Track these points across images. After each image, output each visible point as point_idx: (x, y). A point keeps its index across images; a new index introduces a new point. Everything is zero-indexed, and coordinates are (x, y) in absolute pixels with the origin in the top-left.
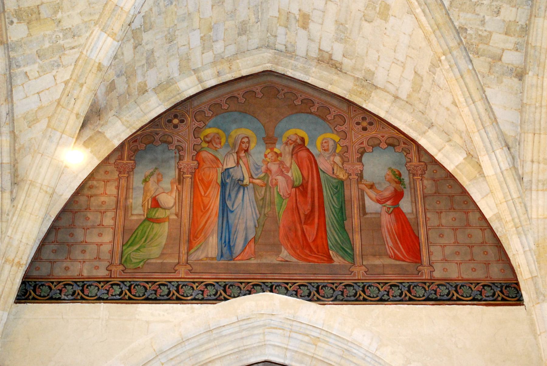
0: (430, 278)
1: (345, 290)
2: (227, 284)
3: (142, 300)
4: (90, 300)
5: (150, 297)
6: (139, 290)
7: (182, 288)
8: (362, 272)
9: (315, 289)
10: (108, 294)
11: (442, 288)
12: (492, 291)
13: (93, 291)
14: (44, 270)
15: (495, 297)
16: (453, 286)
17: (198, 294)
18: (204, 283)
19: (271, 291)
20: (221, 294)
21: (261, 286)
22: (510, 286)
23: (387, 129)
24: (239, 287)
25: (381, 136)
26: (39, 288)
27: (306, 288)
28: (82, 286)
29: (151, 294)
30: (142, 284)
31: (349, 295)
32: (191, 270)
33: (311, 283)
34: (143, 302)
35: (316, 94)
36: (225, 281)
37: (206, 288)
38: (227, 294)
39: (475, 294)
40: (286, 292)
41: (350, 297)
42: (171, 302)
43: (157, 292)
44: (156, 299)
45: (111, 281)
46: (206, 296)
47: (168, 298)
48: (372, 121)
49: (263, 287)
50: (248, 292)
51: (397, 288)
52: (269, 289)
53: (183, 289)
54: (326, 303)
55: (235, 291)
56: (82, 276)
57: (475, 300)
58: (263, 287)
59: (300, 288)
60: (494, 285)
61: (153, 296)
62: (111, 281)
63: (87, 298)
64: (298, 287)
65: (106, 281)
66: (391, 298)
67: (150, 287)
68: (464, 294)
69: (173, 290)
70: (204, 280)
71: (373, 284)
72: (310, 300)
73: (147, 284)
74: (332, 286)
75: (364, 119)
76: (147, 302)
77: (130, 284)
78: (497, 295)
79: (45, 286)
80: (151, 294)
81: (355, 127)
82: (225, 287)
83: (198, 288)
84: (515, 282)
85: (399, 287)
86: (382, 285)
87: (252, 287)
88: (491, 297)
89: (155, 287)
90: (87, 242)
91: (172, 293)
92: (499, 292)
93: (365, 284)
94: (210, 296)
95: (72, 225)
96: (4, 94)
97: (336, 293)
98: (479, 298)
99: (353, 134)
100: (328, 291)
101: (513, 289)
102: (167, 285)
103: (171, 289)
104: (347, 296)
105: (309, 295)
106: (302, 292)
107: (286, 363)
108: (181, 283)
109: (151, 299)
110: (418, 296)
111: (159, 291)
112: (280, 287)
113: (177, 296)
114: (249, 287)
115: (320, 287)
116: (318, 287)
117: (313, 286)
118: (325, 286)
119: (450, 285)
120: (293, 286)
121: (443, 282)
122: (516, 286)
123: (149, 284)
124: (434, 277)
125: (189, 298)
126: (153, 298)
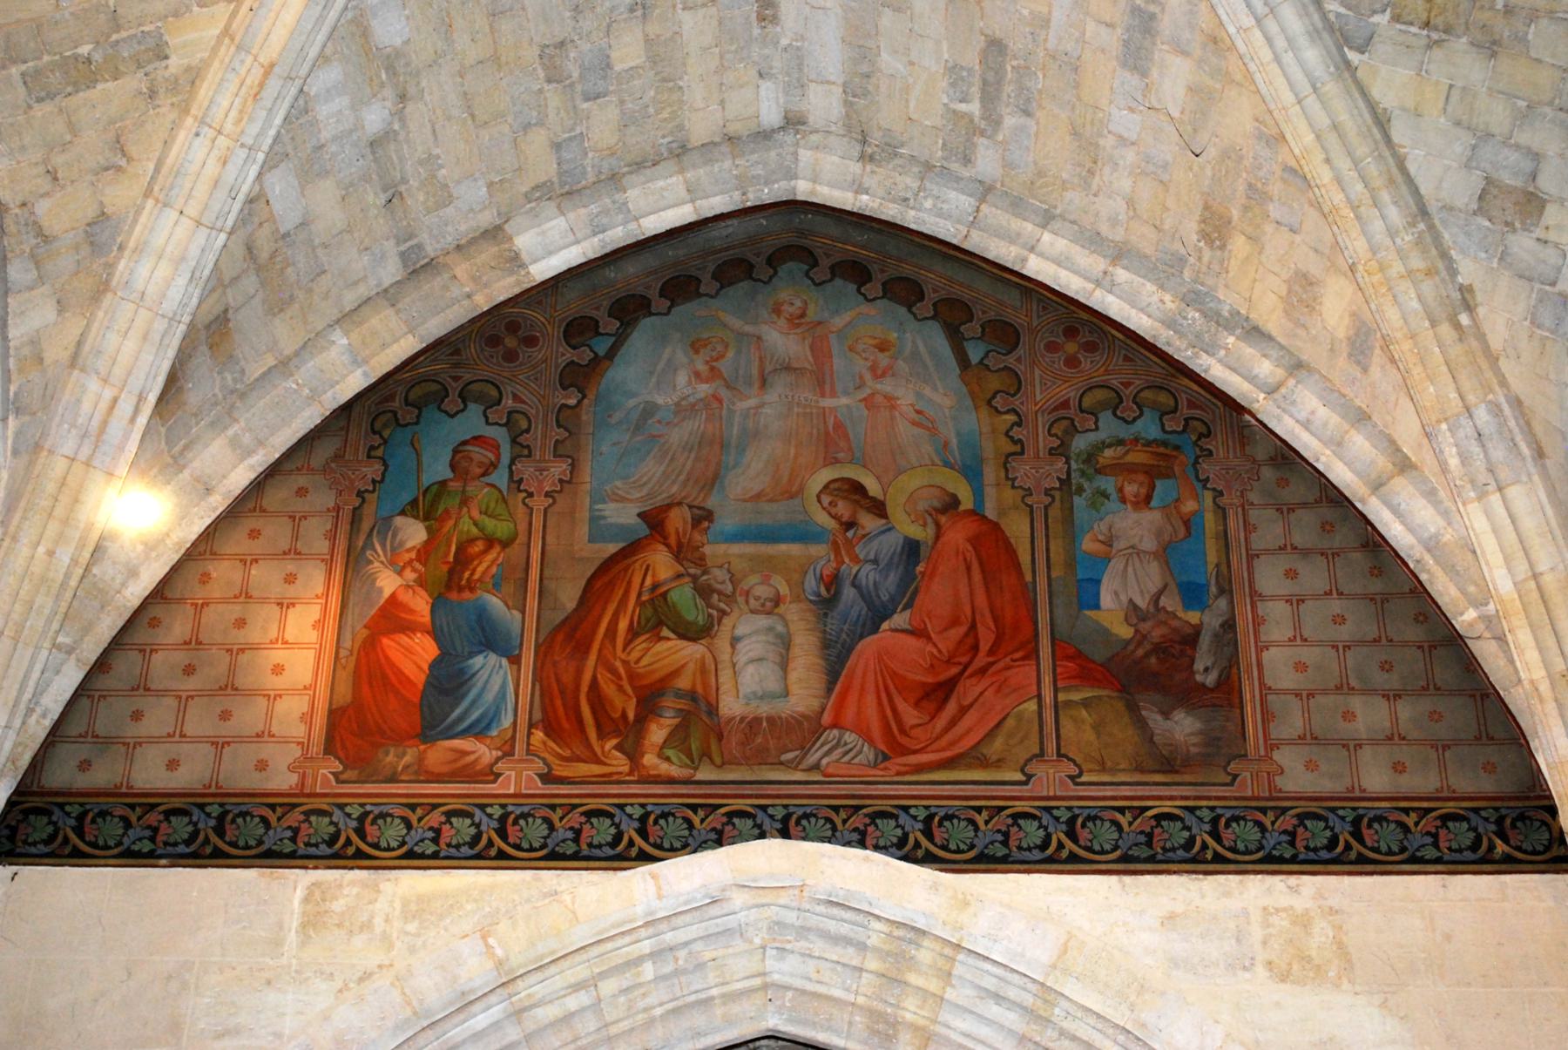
0: (1267, 794)
1: (1157, 831)
2: (88, 811)
3: (966, 862)
4: (954, 862)
5: (136, 848)
6: (535, 831)
7: (940, 824)
8: (1060, 777)
9: (1064, 827)
10: (438, 844)
11: (1030, 826)
12: (1186, 834)
13: (111, 830)
14: (62, 775)
15: (1049, 851)
16: (1492, 820)
17: (422, 840)
18: (723, 810)
19: (785, 834)
20: (1061, 846)
21: (610, 816)
22: (1386, 819)
23: (1139, 362)
24: (688, 821)
25: (1122, 383)
26: (1369, 826)
27: (1465, 825)
28: (923, 821)
29: (140, 839)
30: (1106, 815)
31: (1312, 846)
32: (1080, 775)
33: (910, 807)
34: (542, 864)
35: (671, 252)
36: (785, 802)
37: (167, 819)
38: (652, 840)
39: (561, 838)
40: (829, 833)
41: (1029, 849)
42: (1055, 867)
43: (1298, 839)
44: (576, 856)
45: (1292, 808)
46: (584, 847)
47: (472, 852)
48: (1094, 338)
49: (1473, 824)
50: (713, 836)
51: (1036, 824)
52: (779, 826)
53: (1230, 830)
54: (384, 863)
55: (673, 829)
56: (217, 787)
57: (1412, 860)
58: (617, 820)
59: (1159, 825)
60: (766, 812)
61: (570, 848)
62: (1292, 808)
63: (941, 853)
64: (1154, 823)
65: (852, 806)
66: (1016, 854)
67: (1130, 824)
68: (1095, 842)
69: (630, 831)
70: (165, 800)
71: (1531, 814)
72: (905, 858)
73: (977, 816)
74: (1260, 817)
75: (1071, 332)
76: (268, 862)
77: (642, 811)
78: (1054, 843)
79: (113, 816)
80: (140, 839)
81: (1043, 356)
82: (1071, 821)
83: (847, 825)
84: (1545, 803)
85: (1039, 819)
86: (1129, 816)
87: (725, 819)
88: (323, 847)
89: (436, 818)
90: (236, 689)
91: (202, 836)
92: (1063, 837)
93: (933, 810)
94: (316, 845)
95: (277, 640)
96: (12, 251)
97: (415, 836)
98: (1287, 855)
99: (1037, 376)
100: (1107, 835)
101: (1393, 826)
102: (1466, 819)
103: (623, 827)
104: (1020, 848)
105: (902, 842)
106: (1308, 835)
107: (820, 1037)
108: (1509, 811)
109: (422, 856)
110: (1097, 847)
111: (447, 832)
112: (389, 819)
113: (1071, 852)
114: (716, 819)
115: (1080, 821)
116: (1071, 821)
117: (915, 818)
118: (1093, 818)
119: (1337, 815)
120: (1139, 820)
121: (1313, 807)
122: (1548, 818)
123: (138, 809)
124: (1280, 791)
125: (253, 852)
126: (145, 850)
